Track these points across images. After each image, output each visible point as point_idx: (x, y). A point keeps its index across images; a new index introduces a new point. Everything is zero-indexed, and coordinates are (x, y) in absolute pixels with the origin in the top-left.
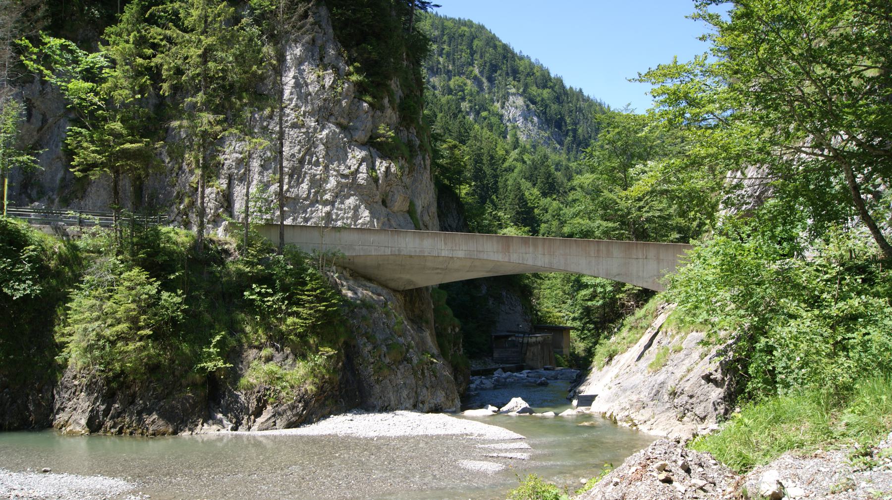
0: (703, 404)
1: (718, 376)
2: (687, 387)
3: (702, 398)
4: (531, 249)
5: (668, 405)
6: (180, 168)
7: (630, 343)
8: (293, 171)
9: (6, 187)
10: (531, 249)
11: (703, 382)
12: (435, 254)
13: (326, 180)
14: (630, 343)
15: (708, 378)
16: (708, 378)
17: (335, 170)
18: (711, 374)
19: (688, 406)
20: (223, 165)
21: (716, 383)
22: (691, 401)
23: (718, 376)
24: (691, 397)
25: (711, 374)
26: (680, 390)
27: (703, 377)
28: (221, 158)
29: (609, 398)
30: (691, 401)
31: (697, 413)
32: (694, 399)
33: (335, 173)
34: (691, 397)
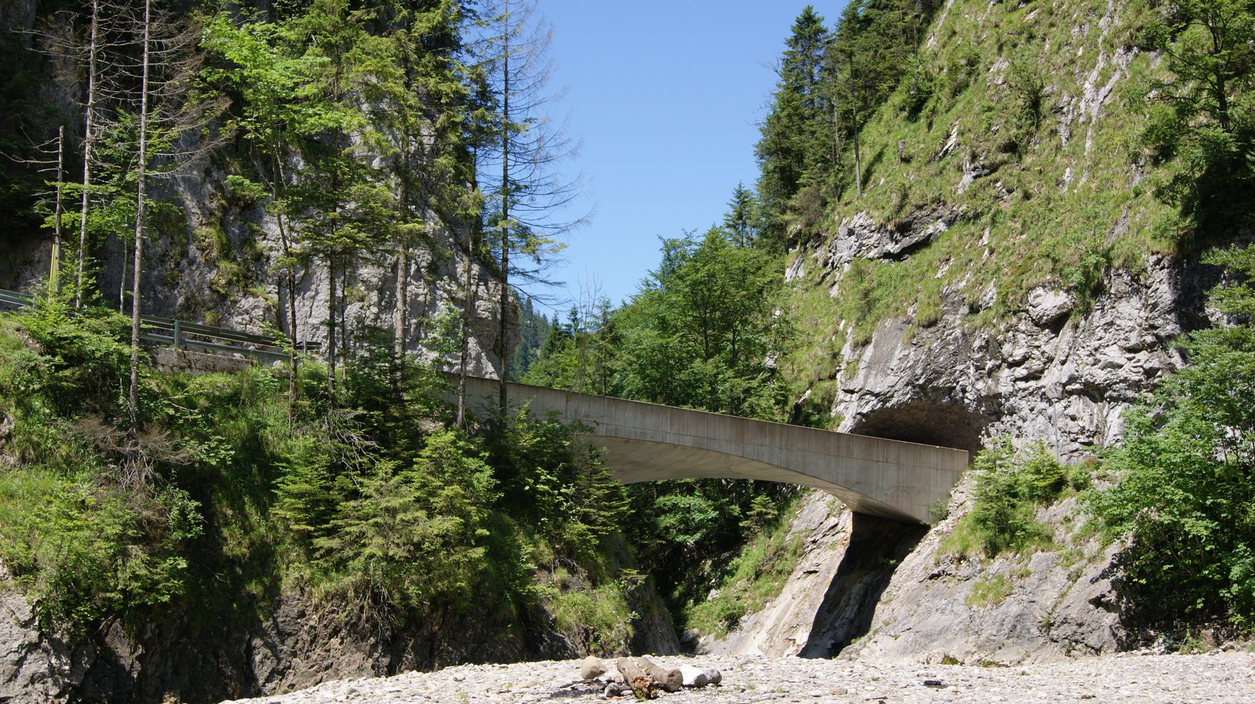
0: (1096, 634)
1: (1112, 597)
2: (1073, 613)
3: (1094, 625)
4: (767, 441)
5: (1041, 640)
6: (184, 254)
7: (766, 594)
8: (384, 284)
9: (137, 261)
10: (767, 441)
11: (1091, 606)
12: (659, 439)
13: (433, 305)
14: (766, 594)
15: (1097, 602)
16: (1097, 602)
17: (445, 291)
18: (1104, 596)
19: (1076, 637)
20: (268, 258)
21: (1108, 607)
22: (1080, 630)
23: (1112, 597)
24: (1080, 625)
25: (1104, 596)
26: (1060, 620)
27: (1090, 602)
28: (262, 245)
29: (905, 648)
30: (1080, 630)
31: (1092, 643)
32: (1084, 629)
33: (445, 295)
34: (1080, 625)
